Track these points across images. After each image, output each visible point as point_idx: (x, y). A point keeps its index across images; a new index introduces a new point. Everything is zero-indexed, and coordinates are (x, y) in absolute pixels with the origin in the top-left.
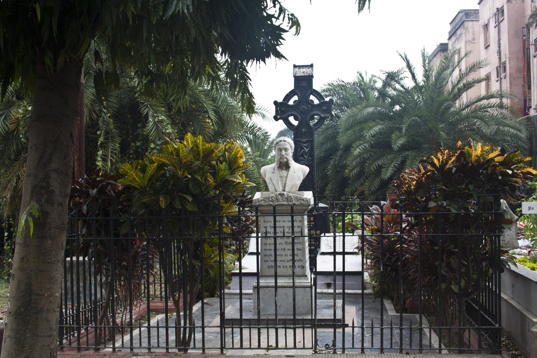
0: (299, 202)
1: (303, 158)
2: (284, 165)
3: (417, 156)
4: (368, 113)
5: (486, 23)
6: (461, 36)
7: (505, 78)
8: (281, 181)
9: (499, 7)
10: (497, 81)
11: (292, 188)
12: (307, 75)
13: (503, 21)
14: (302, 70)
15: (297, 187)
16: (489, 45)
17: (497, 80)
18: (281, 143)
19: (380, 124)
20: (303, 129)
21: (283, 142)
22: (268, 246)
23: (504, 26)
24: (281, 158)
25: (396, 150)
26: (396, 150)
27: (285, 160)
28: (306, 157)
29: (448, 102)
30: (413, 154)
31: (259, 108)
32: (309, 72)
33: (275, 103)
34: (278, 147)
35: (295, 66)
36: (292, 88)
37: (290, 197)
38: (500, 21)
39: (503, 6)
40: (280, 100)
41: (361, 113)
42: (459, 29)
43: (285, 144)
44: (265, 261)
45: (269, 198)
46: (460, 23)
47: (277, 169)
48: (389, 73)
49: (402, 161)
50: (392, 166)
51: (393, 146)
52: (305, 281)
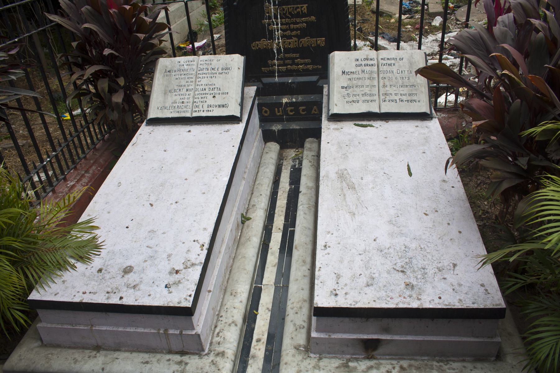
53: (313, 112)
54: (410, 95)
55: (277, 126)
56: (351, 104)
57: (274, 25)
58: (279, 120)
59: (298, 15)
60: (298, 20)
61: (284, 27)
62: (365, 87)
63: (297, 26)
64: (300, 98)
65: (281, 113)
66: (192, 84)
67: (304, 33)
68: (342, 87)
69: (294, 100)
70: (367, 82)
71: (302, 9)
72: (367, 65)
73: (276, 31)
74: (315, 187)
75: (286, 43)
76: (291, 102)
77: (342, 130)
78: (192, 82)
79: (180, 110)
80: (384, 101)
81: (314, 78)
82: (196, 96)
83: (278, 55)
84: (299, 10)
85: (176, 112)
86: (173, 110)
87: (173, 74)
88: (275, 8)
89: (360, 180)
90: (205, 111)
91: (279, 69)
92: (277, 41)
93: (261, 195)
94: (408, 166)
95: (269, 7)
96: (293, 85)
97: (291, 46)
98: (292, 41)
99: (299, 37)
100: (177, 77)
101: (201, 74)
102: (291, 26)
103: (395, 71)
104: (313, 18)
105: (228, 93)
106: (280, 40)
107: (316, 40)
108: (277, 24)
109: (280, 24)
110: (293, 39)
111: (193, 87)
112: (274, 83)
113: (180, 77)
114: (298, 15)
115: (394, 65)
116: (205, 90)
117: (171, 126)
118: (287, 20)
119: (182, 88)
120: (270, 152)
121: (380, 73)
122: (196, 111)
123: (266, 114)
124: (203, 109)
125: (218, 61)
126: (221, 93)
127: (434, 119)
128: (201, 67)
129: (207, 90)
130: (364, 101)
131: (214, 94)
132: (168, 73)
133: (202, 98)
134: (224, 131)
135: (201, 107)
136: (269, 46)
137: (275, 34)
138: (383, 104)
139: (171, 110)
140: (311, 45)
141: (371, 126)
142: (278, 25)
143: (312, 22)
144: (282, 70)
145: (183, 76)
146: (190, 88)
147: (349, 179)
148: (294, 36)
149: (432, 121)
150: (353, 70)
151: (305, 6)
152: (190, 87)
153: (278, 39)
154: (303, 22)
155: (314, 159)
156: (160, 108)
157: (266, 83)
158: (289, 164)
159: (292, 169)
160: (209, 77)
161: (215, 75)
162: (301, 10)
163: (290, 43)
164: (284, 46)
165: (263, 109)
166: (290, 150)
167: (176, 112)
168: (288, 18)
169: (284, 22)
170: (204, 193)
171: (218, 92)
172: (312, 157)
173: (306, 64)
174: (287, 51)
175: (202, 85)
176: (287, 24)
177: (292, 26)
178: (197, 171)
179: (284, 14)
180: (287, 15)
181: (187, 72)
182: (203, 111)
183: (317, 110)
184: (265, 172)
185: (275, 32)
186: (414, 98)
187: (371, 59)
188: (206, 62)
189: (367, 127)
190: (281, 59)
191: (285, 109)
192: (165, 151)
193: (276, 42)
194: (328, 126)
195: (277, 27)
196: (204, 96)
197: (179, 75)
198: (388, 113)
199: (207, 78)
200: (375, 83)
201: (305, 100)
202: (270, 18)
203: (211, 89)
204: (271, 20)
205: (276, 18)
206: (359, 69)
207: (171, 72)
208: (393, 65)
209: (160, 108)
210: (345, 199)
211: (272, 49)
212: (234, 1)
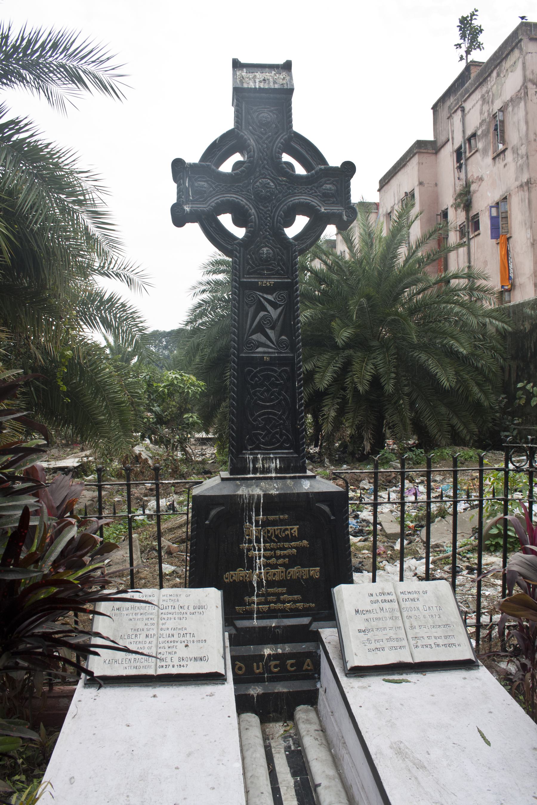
1: (263, 339)
5: (389, 211)
9: (408, 191)
12: (277, 86)
14: (259, 76)
19: (310, 308)
20: (265, 249)
26: (340, 345)
28: (271, 333)
30: (359, 354)
32: (281, 81)
35: (237, 64)
39: (414, 189)
51: (337, 340)
53: (305, 667)
54: (446, 637)
55: (255, 689)
56: (374, 652)
57: (255, 551)
58: (258, 680)
59: (287, 539)
60: (286, 545)
61: (268, 553)
62: (388, 629)
63: (285, 552)
64: (288, 648)
65: (261, 670)
66: (153, 627)
67: (293, 561)
68: (360, 631)
69: (280, 651)
70: (390, 623)
71: (292, 531)
72: (385, 601)
73: (257, 558)
74: (337, 775)
75: (270, 573)
76: (277, 654)
77: (370, 688)
78: (153, 624)
79: (138, 664)
80: (416, 647)
81: (305, 621)
82: (162, 645)
83: (258, 590)
84: (287, 532)
85: (132, 667)
86: (128, 665)
87: (123, 612)
88: (258, 530)
89: (427, 756)
90: (176, 666)
91: (258, 608)
92: (257, 571)
93: (262, 793)
94: (480, 731)
95: (249, 529)
96: (278, 630)
97: (277, 578)
98: (277, 572)
99: (286, 566)
100: (131, 617)
101: (165, 614)
102: (277, 552)
103: (421, 608)
104: (305, 542)
105: (205, 641)
106: (262, 571)
107: (309, 570)
108: (259, 550)
109: (262, 550)
110: (278, 569)
111: (155, 632)
112: (252, 627)
113: (134, 616)
114: (287, 539)
115: (418, 599)
116: (173, 636)
117: (124, 689)
118: (273, 545)
119: (139, 632)
120: (250, 728)
121: (402, 610)
122: (162, 666)
123: (240, 672)
124: (171, 664)
125: (187, 596)
126: (195, 640)
127: (480, 667)
128: (165, 604)
129: (176, 636)
130: (391, 648)
131: (186, 642)
132: (117, 612)
133: (169, 647)
134: (207, 695)
135: (169, 660)
136: (246, 578)
137: (256, 562)
138: (416, 651)
139: (125, 665)
140: (302, 576)
141: (407, 681)
142: (261, 551)
143: (304, 548)
144: (262, 610)
145: (139, 616)
146: (151, 633)
147: (411, 755)
148: (281, 565)
149: (480, 671)
150: (369, 608)
151: (296, 527)
152: (151, 632)
153: (260, 569)
154: (292, 548)
155: (319, 735)
156: (107, 662)
157: (242, 628)
158: (280, 744)
159: (287, 753)
160: (176, 618)
161: (185, 616)
162: (291, 532)
163: (275, 574)
164: (267, 578)
165: (237, 664)
166: (274, 724)
167: (132, 667)
168: (274, 541)
169: (268, 547)
170: (213, 788)
171: (192, 639)
172: (316, 732)
173: (295, 602)
174: (271, 584)
175: (168, 629)
176: (271, 550)
177: (278, 552)
178: (189, 755)
179: (269, 537)
180: (273, 538)
181: (145, 611)
182: (173, 666)
183: (310, 664)
184: (255, 758)
185: (256, 559)
186: (453, 641)
187: (388, 594)
188: (171, 598)
189: (401, 682)
190: (263, 595)
191: (267, 663)
192: (128, 726)
193: (257, 573)
194: (350, 684)
195: (259, 554)
196: (172, 644)
197: (134, 614)
198: (424, 662)
199: (175, 619)
200: (400, 624)
201: (295, 651)
202: (250, 541)
203: (182, 634)
204: (252, 545)
205: (258, 541)
206: (375, 606)
207: (122, 610)
208: (416, 600)
209: (107, 662)
210: (419, 783)
211: (251, 582)
212: (206, 520)
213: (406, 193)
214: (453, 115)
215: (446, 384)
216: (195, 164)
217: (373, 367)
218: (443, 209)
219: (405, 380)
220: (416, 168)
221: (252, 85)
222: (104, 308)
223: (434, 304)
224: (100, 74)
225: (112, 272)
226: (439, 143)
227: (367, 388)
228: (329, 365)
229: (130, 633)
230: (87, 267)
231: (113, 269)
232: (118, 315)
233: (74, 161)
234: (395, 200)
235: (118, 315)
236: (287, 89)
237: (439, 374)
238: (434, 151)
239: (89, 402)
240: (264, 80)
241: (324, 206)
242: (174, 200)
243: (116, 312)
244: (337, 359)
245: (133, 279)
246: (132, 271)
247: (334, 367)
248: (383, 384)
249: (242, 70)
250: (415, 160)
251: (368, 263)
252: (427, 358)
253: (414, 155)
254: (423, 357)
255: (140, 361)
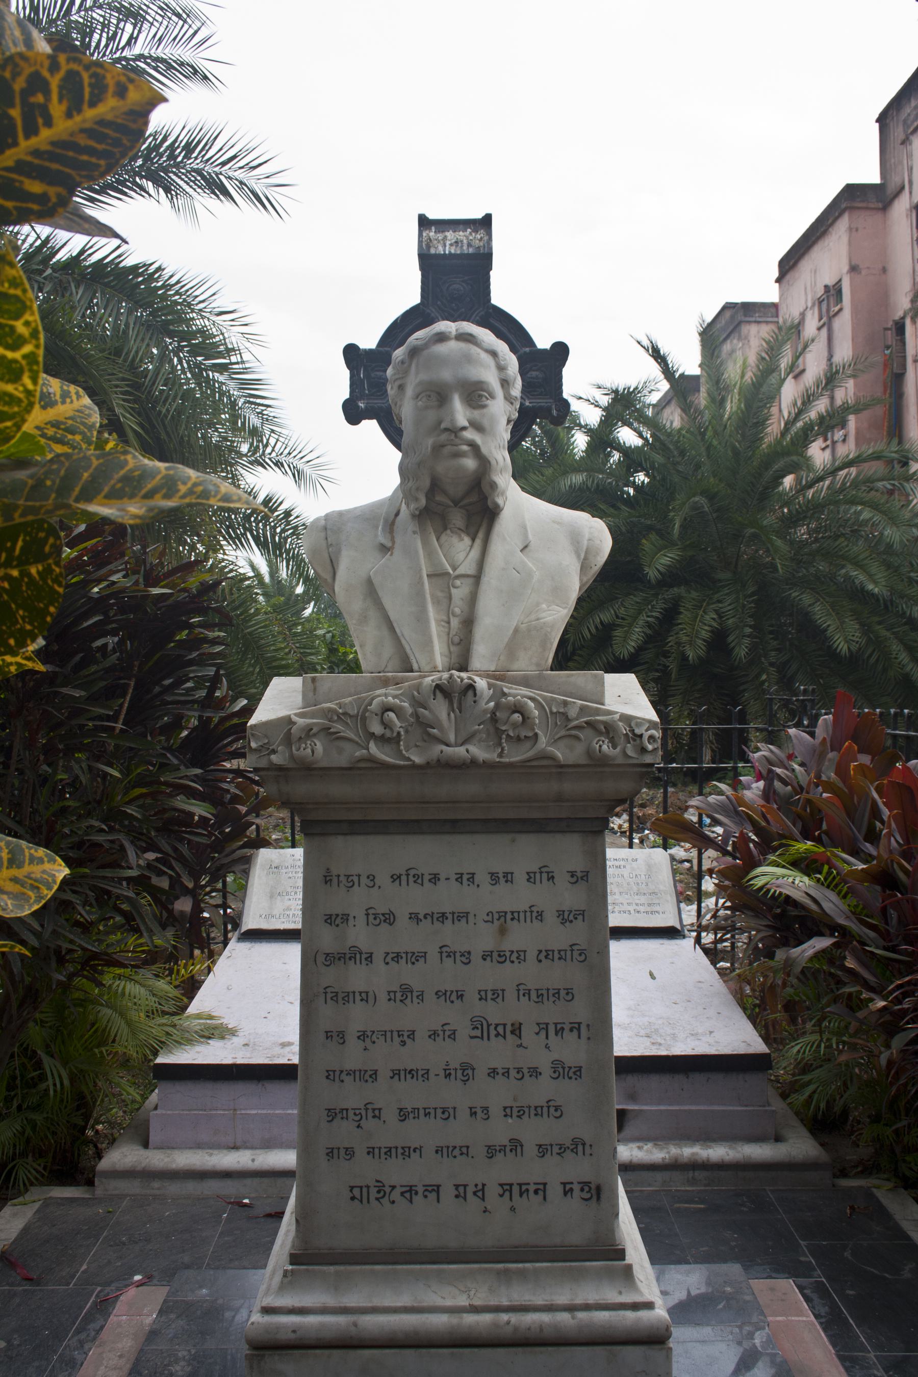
0: (580, 749)
2: (456, 503)
3: (704, 600)
4: (570, 486)
6: (734, 356)
7: (844, 441)
8: (436, 602)
9: (830, 281)
10: (823, 449)
11: (512, 649)
12: (471, 250)
13: (841, 314)
15: (544, 643)
16: (803, 371)
17: (823, 445)
18: (442, 349)
21: (453, 345)
22: (353, 1045)
23: (844, 324)
24: (438, 449)
25: (653, 581)
26: (653, 581)
27: (470, 463)
29: (787, 459)
30: (694, 594)
31: (286, 451)
32: (477, 243)
33: (351, 353)
34: (423, 376)
35: (424, 222)
36: (414, 298)
37: (518, 709)
38: (832, 313)
39: (840, 280)
40: (369, 341)
41: (553, 488)
42: (729, 341)
43: (468, 359)
44: (331, 1153)
45: (362, 719)
46: (731, 328)
47: (412, 526)
48: (616, 392)
49: (665, 609)
50: (641, 623)
51: (647, 570)
52: (612, 1295)
54: (649, 905)
100: (290, 875)
115: (624, 867)
213: (826, 286)
214: (911, 137)
215: (842, 647)
216: (371, 350)
217: (715, 616)
218: (897, 318)
219: (772, 639)
220: (845, 239)
221: (441, 250)
222: (256, 519)
223: (829, 504)
224: (252, 183)
225: (270, 459)
226: (891, 189)
227: (701, 653)
228: (639, 614)
229: (289, 890)
230: (230, 451)
231: (270, 454)
232: (278, 530)
233: (214, 294)
234: (806, 300)
235: (278, 530)
236: (483, 254)
237: (831, 629)
238: (880, 205)
239: (232, 666)
240: (456, 242)
241: (529, 398)
242: (346, 395)
243: (275, 525)
244: (654, 603)
245: (303, 471)
246: (302, 458)
247: (648, 616)
248: (732, 645)
249: (430, 230)
250: (843, 225)
251: (716, 433)
252: (812, 601)
253: (841, 214)
254: (807, 599)
255: (317, 613)
